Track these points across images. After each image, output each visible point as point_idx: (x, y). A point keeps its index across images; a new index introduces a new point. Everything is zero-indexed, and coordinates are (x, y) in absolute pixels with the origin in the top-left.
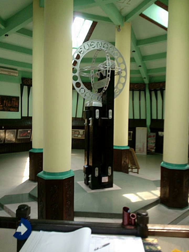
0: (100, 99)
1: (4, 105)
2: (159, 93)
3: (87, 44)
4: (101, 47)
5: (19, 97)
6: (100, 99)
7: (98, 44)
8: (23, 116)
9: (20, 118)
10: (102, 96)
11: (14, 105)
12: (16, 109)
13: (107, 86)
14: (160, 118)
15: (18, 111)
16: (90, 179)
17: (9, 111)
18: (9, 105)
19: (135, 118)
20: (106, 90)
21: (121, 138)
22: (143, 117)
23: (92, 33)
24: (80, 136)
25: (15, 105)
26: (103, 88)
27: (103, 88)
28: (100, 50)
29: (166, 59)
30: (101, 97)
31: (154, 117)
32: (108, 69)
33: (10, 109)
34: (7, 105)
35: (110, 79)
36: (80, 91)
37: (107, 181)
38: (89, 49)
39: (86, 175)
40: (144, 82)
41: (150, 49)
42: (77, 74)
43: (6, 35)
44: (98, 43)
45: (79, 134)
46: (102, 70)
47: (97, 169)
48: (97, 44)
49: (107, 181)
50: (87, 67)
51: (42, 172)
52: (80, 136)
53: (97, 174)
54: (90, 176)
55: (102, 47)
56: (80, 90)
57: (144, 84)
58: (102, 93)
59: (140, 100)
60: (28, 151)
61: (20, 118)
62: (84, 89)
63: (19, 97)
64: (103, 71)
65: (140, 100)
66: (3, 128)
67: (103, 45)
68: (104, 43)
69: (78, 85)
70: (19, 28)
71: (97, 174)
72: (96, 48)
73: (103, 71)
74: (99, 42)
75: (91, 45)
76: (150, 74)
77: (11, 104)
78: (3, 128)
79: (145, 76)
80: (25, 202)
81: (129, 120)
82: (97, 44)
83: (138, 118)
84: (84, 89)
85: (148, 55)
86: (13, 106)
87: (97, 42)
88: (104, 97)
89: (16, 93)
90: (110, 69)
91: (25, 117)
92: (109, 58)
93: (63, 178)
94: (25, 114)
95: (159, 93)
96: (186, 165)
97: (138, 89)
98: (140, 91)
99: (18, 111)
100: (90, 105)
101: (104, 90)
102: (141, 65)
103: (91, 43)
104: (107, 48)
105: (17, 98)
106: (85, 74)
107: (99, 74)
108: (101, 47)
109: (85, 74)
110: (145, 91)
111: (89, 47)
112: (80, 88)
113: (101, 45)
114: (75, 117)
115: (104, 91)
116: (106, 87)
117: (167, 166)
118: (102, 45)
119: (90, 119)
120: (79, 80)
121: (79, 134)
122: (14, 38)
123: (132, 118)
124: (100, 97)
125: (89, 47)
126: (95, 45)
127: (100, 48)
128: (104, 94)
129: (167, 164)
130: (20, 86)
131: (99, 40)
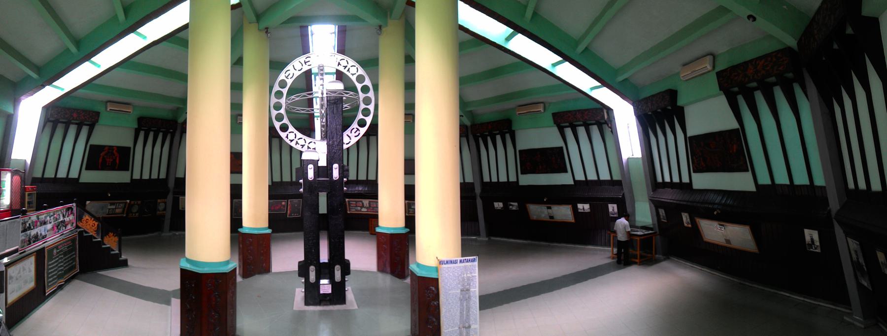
2: (508, 136)
8: (274, 180)
14: (372, 177)
19: (284, 180)
24: (364, 210)
31: (486, 179)
37: (615, 206)
42: (282, 111)
45: (363, 206)
49: (615, 206)
50: (295, 98)
52: (364, 210)
76: (469, 109)
80: (314, 312)
83: (506, 180)
91: (277, 183)
94: (136, 176)
95: (508, 136)
114: (53, 176)
121: (363, 206)
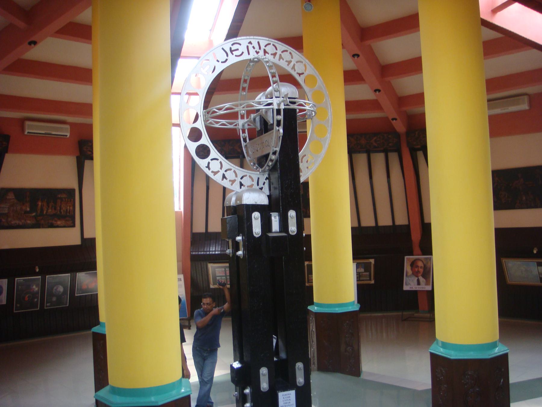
0: (264, 184)
1: (39, 212)
3: (257, 41)
4: (259, 54)
5: (74, 190)
6: (264, 184)
7: (250, 47)
9: (78, 242)
10: (269, 175)
11: (62, 211)
12: (68, 219)
13: (278, 149)
15: (74, 226)
16: (249, 398)
17: (52, 226)
18: (50, 210)
19: (381, 223)
20: (277, 161)
21: (336, 279)
22: (401, 220)
23: (243, 20)
25: (67, 210)
26: (267, 156)
27: (267, 156)
28: (256, 60)
29: (92, 118)
30: (267, 179)
32: (275, 107)
33: (54, 222)
34: (45, 212)
35: (281, 131)
36: (208, 167)
38: (227, 60)
39: (238, 388)
40: (394, 128)
41: (393, 49)
43: (30, 43)
44: (250, 43)
46: (264, 110)
47: (264, 371)
48: (248, 47)
51: (107, 388)
53: (264, 385)
54: (247, 391)
55: (261, 53)
56: (209, 163)
57: (397, 135)
58: (267, 168)
59: (388, 176)
60: (90, 328)
61: (78, 242)
62: (218, 162)
63: (74, 190)
64: (266, 112)
65: (388, 176)
66: (37, 270)
67: (263, 47)
68: (267, 42)
69: (203, 152)
70: (60, 23)
71: (264, 385)
72: (245, 57)
73: (266, 112)
74: (252, 41)
75: (232, 51)
77: (55, 209)
78: (37, 270)
79: (395, 115)
81: (353, 229)
82: (248, 47)
84: (218, 162)
85: (392, 62)
86: (61, 212)
87: (249, 41)
88: (272, 177)
89: (68, 181)
90: (282, 107)
92: (277, 78)
93: (157, 402)
96: (494, 345)
97: (382, 149)
98: (386, 152)
99: (74, 226)
100: (236, 200)
101: (271, 160)
102: (379, 87)
103: (232, 45)
104: (275, 54)
105: (70, 192)
106: (224, 121)
107: (258, 119)
108: (257, 53)
109: (219, 124)
110: (399, 151)
111: (227, 56)
112: (208, 159)
113: (257, 49)
115: (270, 164)
116: (274, 153)
117: (447, 351)
118: (260, 48)
119: (239, 238)
120: (205, 140)
122: (53, 49)
123: (356, 225)
124: (263, 179)
125: (227, 56)
126: (242, 48)
127: (256, 55)
128: (273, 169)
129: (445, 345)
130: (76, 160)
131: (251, 37)
